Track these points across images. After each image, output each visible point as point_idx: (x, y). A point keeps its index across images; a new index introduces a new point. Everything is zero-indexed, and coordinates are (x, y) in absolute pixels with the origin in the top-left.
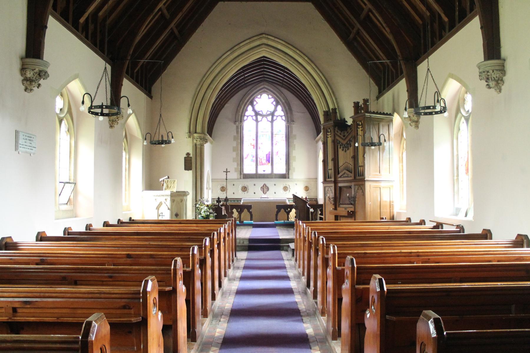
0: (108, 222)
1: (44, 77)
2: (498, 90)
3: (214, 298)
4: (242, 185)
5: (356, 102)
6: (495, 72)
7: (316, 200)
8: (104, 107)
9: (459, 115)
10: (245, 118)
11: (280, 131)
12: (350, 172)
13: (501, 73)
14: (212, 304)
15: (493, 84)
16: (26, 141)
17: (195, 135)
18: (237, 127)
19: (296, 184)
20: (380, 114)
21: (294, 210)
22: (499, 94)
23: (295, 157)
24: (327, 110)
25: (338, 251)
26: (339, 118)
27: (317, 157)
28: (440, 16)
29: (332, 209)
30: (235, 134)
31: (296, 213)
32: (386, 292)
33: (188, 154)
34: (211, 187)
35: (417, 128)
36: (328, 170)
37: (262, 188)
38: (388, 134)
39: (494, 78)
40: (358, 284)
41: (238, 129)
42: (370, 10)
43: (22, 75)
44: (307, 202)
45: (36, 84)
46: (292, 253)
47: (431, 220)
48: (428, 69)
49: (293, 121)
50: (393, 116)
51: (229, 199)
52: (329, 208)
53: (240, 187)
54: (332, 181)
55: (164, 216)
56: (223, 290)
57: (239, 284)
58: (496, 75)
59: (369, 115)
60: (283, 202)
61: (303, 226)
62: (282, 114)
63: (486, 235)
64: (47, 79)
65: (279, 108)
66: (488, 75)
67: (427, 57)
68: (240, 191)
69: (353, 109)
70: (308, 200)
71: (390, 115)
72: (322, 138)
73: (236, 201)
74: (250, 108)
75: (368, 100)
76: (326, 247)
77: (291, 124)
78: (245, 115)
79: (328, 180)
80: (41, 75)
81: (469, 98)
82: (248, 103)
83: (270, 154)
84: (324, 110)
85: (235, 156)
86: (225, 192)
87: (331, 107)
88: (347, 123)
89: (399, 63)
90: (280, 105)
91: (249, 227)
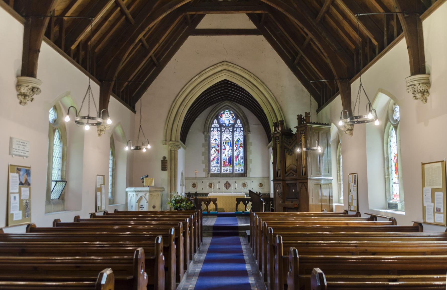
0: (59, 220)
1: (36, 93)
2: (424, 101)
3: (178, 280)
4: (210, 182)
5: (299, 115)
6: (421, 85)
7: (269, 194)
8: (87, 118)
9: (389, 123)
10: (212, 130)
11: (240, 139)
12: (295, 172)
13: (427, 86)
14: (177, 286)
15: (419, 96)
16: (19, 146)
17: (170, 142)
18: (205, 137)
19: (252, 182)
20: (320, 124)
21: (250, 203)
22: (425, 104)
23: (251, 160)
24: (276, 121)
25: (283, 241)
26: (286, 129)
28: (370, 40)
29: (281, 202)
31: (252, 205)
32: (326, 287)
33: (164, 158)
34: (184, 184)
35: (351, 135)
36: (277, 170)
37: (225, 185)
38: (327, 141)
39: (420, 90)
40: (301, 273)
42: (311, 40)
43: (17, 90)
44: (261, 197)
45: (30, 99)
46: (248, 238)
47: (366, 213)
48: (361, 84)
49: (250, 131)
50: (331, 126)
51: (199, 193)
52: (279, 201)
54: (280, 179)
55: (144, 208)
56: (188, 272)
57: (202, 267)
58: (422, 88)
59: (310, 125)
60: (243, 196)
61: (256, 217)
62: (241, 126)
63: (418, 227)
64: (39, 94)
65: (239, 121)
66: (415, 88)
67: (360, 75)
68: (208, 187)
69: (297, 121)
70: (261, 195)
71: (328, 125)
72: (272, 144)
73: (202, 195)
74: (215, 121)
75: (309, 113)
76: (274, 237)
77: (248, 134)
78: (211, 127)
79: (277, 178)
80: (34, 90)
81: (397, 109)
82: (214, 117)
83: (231, 158)
84: (274, 122)
85: (203, 159)
86: (195, 188)
87: (279, 119)
88: (292, 132)
89: (335, 83)
90: (239, 119)
91: (215, 216)
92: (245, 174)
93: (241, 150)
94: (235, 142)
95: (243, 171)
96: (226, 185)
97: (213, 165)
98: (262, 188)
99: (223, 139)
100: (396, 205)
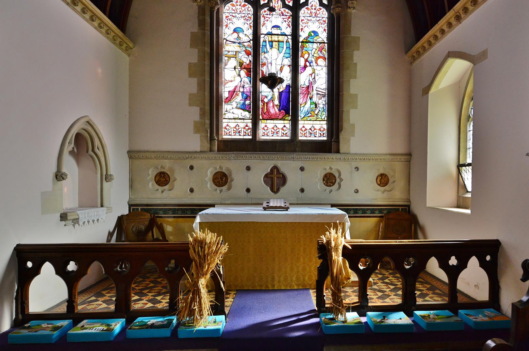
4: (216, 169)
19: (357, 169)
27: (13, 302)
30: (196, 29)
41: (204, 15)
53: (209, 173)
68: (210, 185)
92: (333, 144)
93: (319, 68)
94: (302, 42)
95: (326, 135)
96: (272, 179)
97: (231, 116)
99: (264, 30)
100: (332, 169)
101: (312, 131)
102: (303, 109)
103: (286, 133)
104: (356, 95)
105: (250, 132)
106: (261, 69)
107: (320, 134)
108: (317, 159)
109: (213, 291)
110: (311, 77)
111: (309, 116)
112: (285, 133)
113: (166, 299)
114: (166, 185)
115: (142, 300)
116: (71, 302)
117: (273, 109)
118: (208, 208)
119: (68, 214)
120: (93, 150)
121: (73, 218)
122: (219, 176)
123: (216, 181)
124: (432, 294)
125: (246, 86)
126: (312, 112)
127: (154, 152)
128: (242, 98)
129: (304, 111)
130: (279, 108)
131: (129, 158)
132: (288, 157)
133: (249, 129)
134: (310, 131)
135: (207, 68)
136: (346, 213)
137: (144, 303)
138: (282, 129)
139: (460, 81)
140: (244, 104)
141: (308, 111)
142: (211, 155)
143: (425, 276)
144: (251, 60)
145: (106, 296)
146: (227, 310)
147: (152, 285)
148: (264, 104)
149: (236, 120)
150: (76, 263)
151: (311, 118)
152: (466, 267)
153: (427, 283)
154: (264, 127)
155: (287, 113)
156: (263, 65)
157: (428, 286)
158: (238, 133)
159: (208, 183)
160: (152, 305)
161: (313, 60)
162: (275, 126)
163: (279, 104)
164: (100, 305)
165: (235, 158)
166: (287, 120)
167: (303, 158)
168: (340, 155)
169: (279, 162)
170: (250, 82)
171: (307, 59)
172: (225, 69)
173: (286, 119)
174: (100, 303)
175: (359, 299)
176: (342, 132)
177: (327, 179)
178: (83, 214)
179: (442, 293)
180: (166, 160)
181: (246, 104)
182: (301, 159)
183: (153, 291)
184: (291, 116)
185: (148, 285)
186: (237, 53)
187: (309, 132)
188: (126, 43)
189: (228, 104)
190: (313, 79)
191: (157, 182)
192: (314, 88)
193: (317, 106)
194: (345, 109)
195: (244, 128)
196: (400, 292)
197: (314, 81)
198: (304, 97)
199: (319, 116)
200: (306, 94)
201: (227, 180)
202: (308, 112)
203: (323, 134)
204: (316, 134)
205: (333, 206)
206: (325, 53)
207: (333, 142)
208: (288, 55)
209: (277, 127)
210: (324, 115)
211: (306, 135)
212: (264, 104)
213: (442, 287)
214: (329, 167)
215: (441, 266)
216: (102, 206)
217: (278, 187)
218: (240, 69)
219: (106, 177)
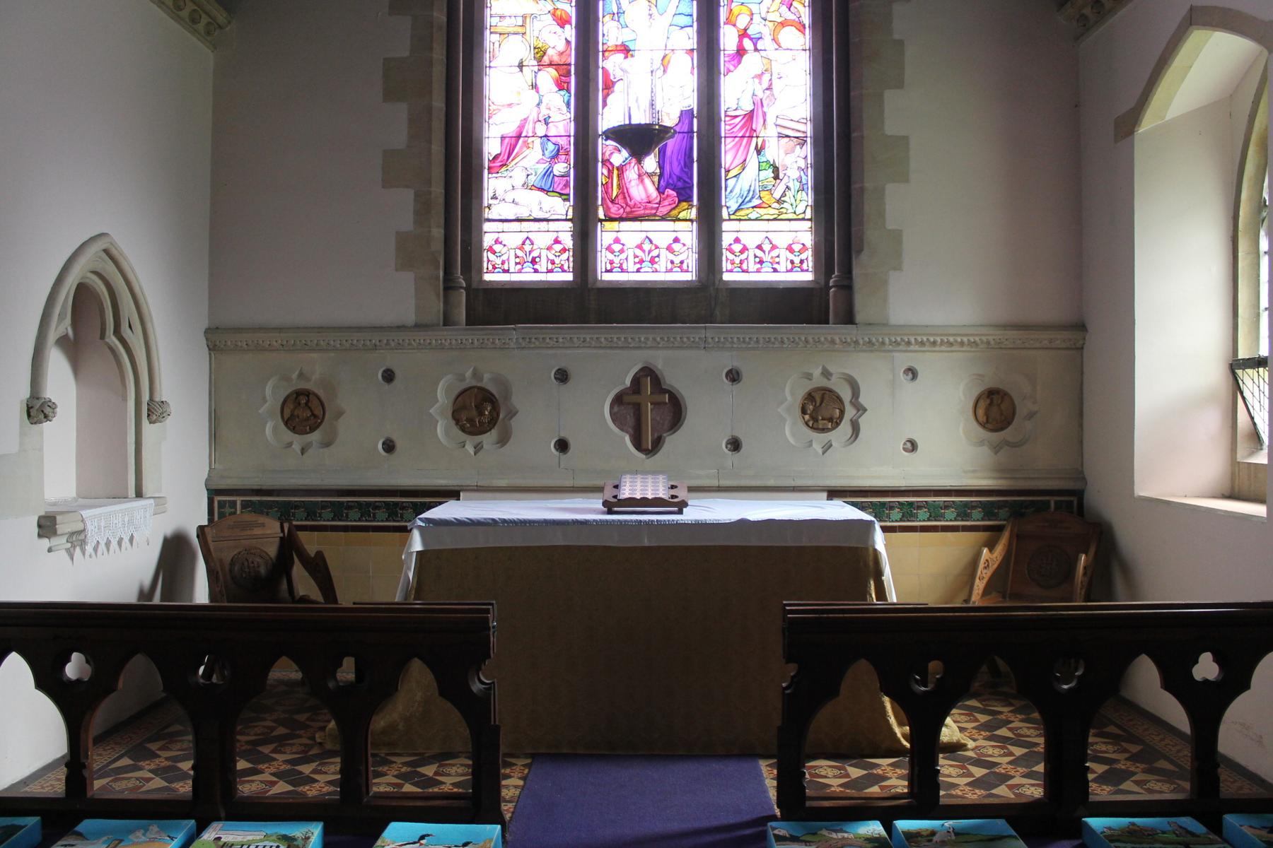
4: (461, 378)
85: (398, 136)
95: (809, 264)
96: (638, 410)
98: (1007, 443)
100: (831, 375)
101: (764, 252)
102: (735, 185)
103: (682, 262)
104: (905, 139)
105: (568, 259)
106: (600, 65)
107: (792, 262)
108: (783, 342)
109: (460, 754)
110: (760, 83)
111: (753, 207)
112: (677, 260)
113: (326, 773)
114: (312, 430)
115: (261, 772)
116: (75, 764)
117: (641, 187)
118: (441, 503)
119: (59, 518)
120: (117, 331)
121: (70, 530)
122: (473, 400)
123: (464, 416)
124: (1145, 771)
125: (555, 117)
126: (763, 194)
127: (280, 329)
128: (541, 157)
129: (737, 191)
130: (659, 182)
131: (209, 349)
132: (688, 338)
133: (564, 250)
134: (759, 253)
135: (439, 72)
136: (873, 519)
137: (268, 781)
138: (669, 249)
139: (1231, 95)
140: (548, 173)
141: (752, 189)
142: (448, 336)
143: (1157, 738)
144: (569, 39)
145: (160, 757)
146: (507, 809)
147: (281, 730)
148: (611, 173)
149: (525, 224)
150: (89, 658)
151: (761, 211)
152: (1246, 686)
153: (1133, 739)
154: (610, 245)
155: (684, 196)
156: (607, 54)
157: (1135, 749)
158: (531, 265)
159: (437, 422)
160: (290, 788)
161: (766, 31)
162: (647, 240)
163: (658, 171)
164: (148, 780)
165: (520, 344)
166: (686, 220)
167: (735, 340)
168: (855, 332)
169: (661, 354)
170: (568, 105)
171: (745, 30)
172: (492, 69)
173: (682, 216)
174: (148, 776)
175: (911, 786)
176: (864, 256)
177: (816, 409)
178: (96, 520)
179: (1177, 770)
180: (315, 355)
181: (556, 172)
182: (730, 346)
183: (288, 749)
184: (699, 210)
185: (272, 732)
186: (528, 20)
187: (756, 257)
188: (206, 13)
189: (499, 175)
190: (767, 89)
191: (288, 419)
192: (771, 119)
193: (781, 176)
194: (869, 185)
195: (549, 248)
196: (1040, 768)
197: (768, 96)
198: (738, 147)
199: (785, 205)
200: (743, 137)
201: (495, 415)
202: (751, 193)
203: (802, 262)
204: (778, 263)
205: (833, 493)
206: (803, 8)
207: (833, 289)
208: (687, 20)
209: (651, 242)
210: (804, 202)
211: (745, 266)
212: (611, 173)
213: (1179, 751)
214: (819, 370)
215: (1168, 685)
216: (139, 494)
217: (656, 436)
218: (536, 69)
219: (148, 410)
